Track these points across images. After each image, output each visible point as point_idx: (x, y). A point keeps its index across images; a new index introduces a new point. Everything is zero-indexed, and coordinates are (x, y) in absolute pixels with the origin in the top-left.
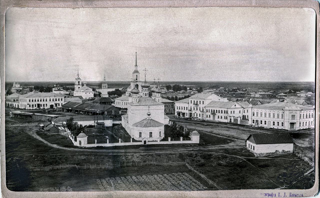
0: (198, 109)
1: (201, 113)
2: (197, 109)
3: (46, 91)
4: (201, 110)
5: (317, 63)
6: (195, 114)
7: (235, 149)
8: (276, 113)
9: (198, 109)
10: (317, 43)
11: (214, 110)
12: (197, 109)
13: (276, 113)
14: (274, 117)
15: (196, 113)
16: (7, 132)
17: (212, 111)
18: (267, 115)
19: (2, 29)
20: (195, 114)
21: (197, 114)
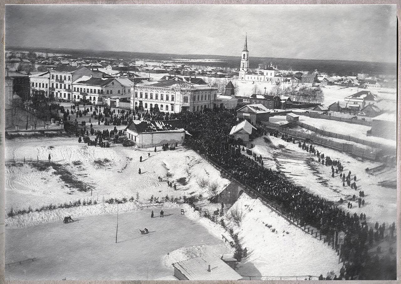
0: (63, 87)
1: (67, 93)
2: (61, 88)
3: (372, 83)
4: (67, 88)
5: (399, 69)
6: (59, 94)
7: (36, 226)
8: (144, 91)
9: (63, 87)
10: (399, 61)
11: (81, 89)
12: (61, 88)
13: (144, 91)
14: (157, 98)
15: (59, 92)
16: (283, 1)
17: (81, 90)
18: (159, 98)
19: (2, 40)
20: (59, 94)
21: (61, 94)
